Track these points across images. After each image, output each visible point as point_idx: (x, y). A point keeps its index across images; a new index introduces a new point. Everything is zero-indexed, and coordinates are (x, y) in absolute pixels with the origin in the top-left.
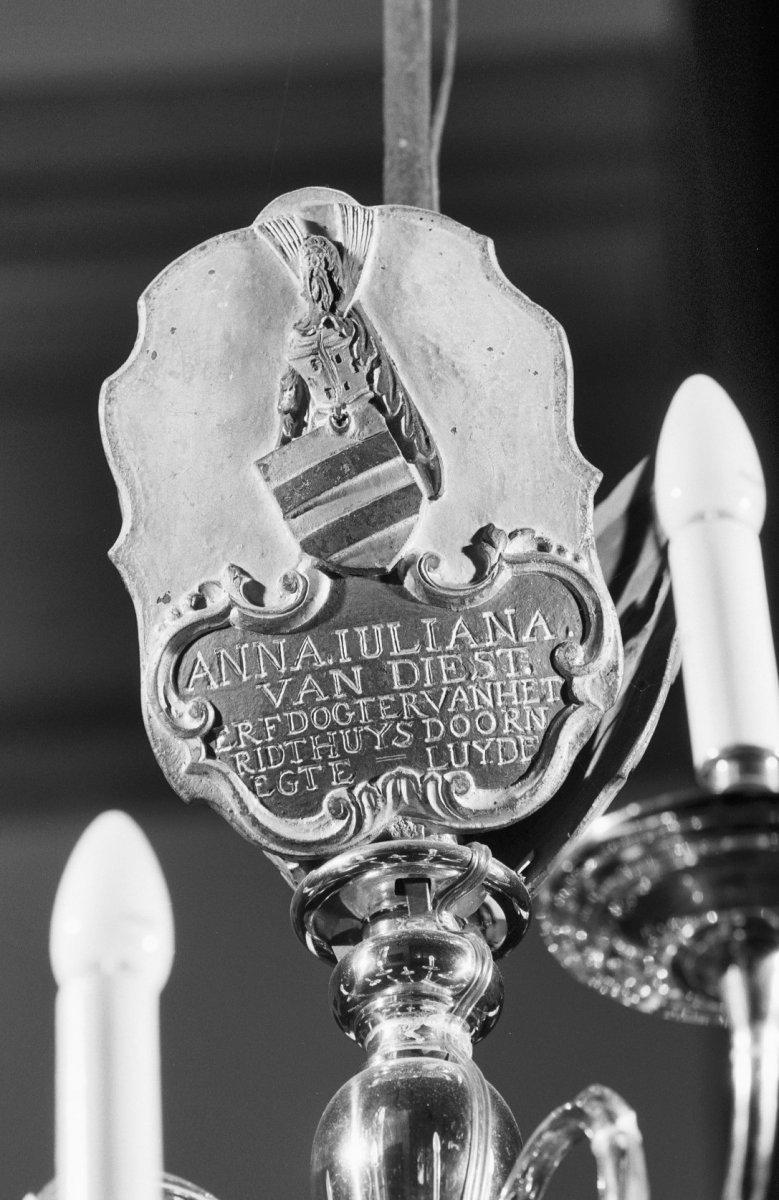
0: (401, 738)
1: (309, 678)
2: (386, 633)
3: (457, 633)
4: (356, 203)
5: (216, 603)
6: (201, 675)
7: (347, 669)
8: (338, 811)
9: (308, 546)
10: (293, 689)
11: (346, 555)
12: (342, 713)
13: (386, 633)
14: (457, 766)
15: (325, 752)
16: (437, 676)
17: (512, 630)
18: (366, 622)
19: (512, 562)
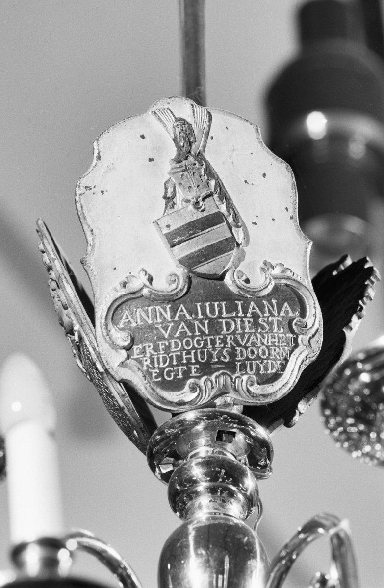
0: (225, 357)
1: (183, 324)
2: (220, 306)
3: (180, 312)
4: (196, 105)
5: (135, 285)
6: (127, 320)
7: (201, 321)
8: (193, 389)
9: (181, 262)
10: (175, 329)
11: (203, 269)
12: (198, 342)
13: (220, 306)
14: (249, 372)
15: (189, 360)
16: (243, 328)
17: (158, 314)
18: (211, 301)
19: (275, 278)
